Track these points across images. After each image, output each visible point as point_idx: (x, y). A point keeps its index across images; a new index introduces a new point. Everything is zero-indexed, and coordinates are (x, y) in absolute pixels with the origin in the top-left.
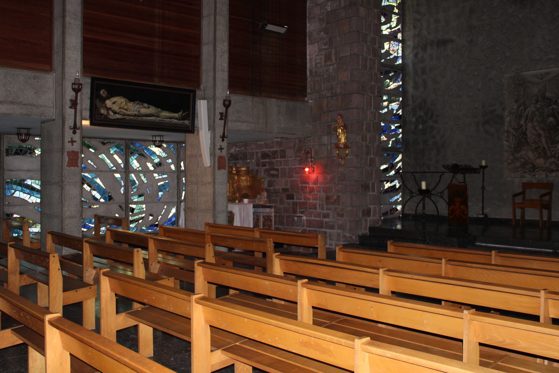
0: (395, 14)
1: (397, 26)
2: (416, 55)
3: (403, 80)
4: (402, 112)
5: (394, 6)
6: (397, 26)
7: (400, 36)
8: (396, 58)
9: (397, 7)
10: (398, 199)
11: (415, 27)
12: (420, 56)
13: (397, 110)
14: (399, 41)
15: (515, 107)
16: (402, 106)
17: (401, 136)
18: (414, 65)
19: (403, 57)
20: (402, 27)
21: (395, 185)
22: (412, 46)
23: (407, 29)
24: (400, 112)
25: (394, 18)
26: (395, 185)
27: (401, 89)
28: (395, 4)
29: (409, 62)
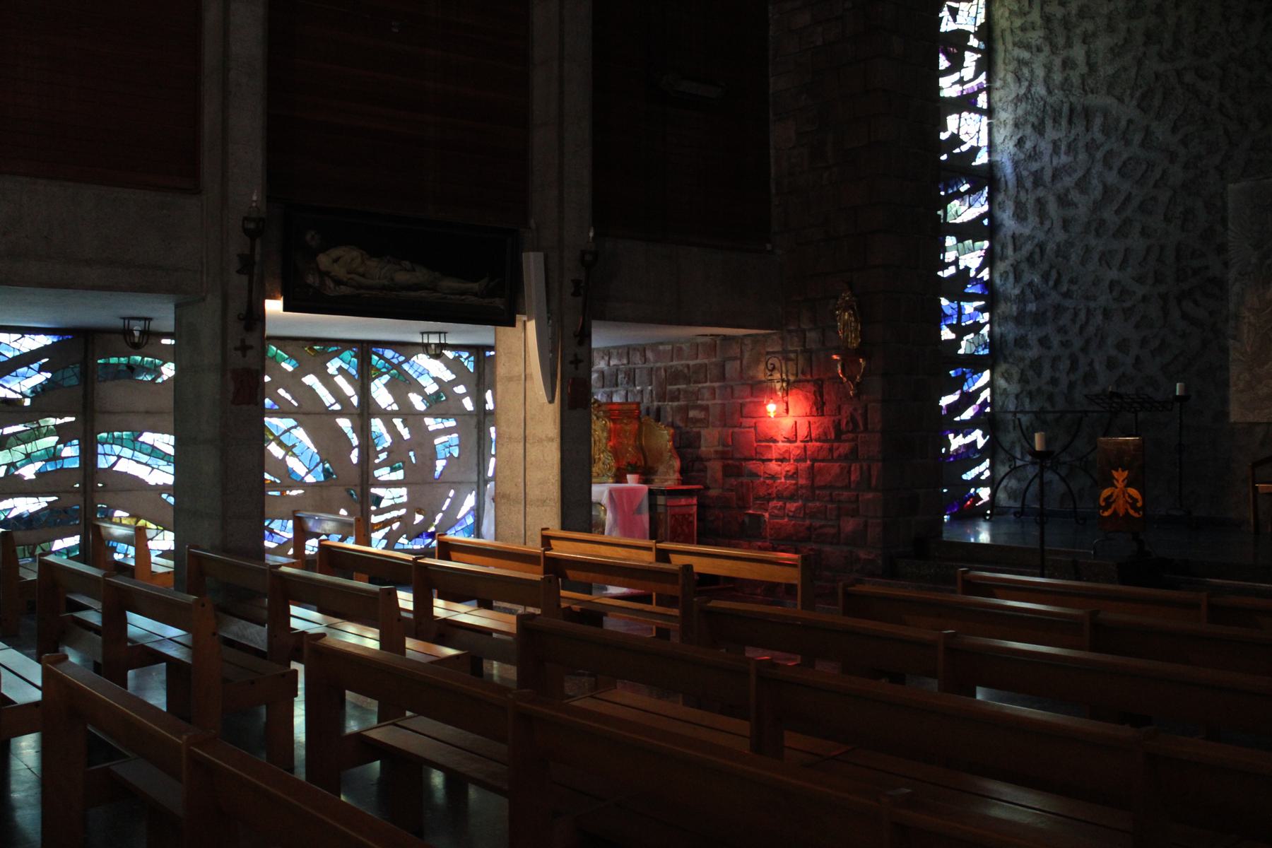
0: (972, 49)
1: (976, 76)
2: (1020, 143)
3: (990, 200)
4: (991, 273)
5: (969, 33)
6: (976, 76)
7: (982, 101)
8: (974, 151)
9: (976, 35)
10: (982, 474)
11: (1019, 79)
12: (1028, 145)
13: (979, 270)
14: (980, 112)
15: (1254, 260)
16: (989, 260)
17: (987, 328)
18: (1016, 164)
19: (991, 147)
20: (989, 79)
21: (975, 442)
22: (1010, 122)
23: (998, 84)
24: (985, 274)
25: (970, 59)
26: (975, 442)
27: (986, 222)
28: (972, 29)
29: (1005, 158)
